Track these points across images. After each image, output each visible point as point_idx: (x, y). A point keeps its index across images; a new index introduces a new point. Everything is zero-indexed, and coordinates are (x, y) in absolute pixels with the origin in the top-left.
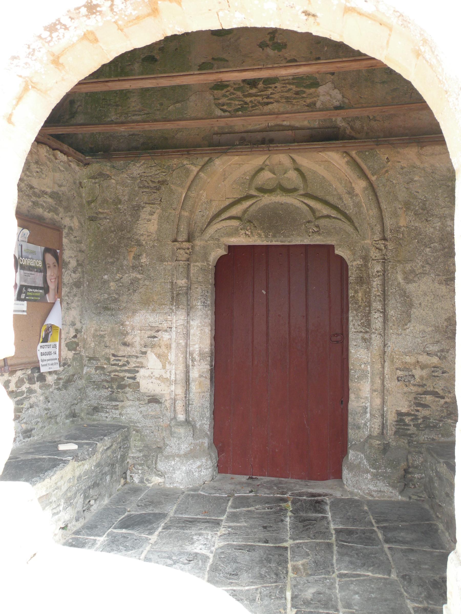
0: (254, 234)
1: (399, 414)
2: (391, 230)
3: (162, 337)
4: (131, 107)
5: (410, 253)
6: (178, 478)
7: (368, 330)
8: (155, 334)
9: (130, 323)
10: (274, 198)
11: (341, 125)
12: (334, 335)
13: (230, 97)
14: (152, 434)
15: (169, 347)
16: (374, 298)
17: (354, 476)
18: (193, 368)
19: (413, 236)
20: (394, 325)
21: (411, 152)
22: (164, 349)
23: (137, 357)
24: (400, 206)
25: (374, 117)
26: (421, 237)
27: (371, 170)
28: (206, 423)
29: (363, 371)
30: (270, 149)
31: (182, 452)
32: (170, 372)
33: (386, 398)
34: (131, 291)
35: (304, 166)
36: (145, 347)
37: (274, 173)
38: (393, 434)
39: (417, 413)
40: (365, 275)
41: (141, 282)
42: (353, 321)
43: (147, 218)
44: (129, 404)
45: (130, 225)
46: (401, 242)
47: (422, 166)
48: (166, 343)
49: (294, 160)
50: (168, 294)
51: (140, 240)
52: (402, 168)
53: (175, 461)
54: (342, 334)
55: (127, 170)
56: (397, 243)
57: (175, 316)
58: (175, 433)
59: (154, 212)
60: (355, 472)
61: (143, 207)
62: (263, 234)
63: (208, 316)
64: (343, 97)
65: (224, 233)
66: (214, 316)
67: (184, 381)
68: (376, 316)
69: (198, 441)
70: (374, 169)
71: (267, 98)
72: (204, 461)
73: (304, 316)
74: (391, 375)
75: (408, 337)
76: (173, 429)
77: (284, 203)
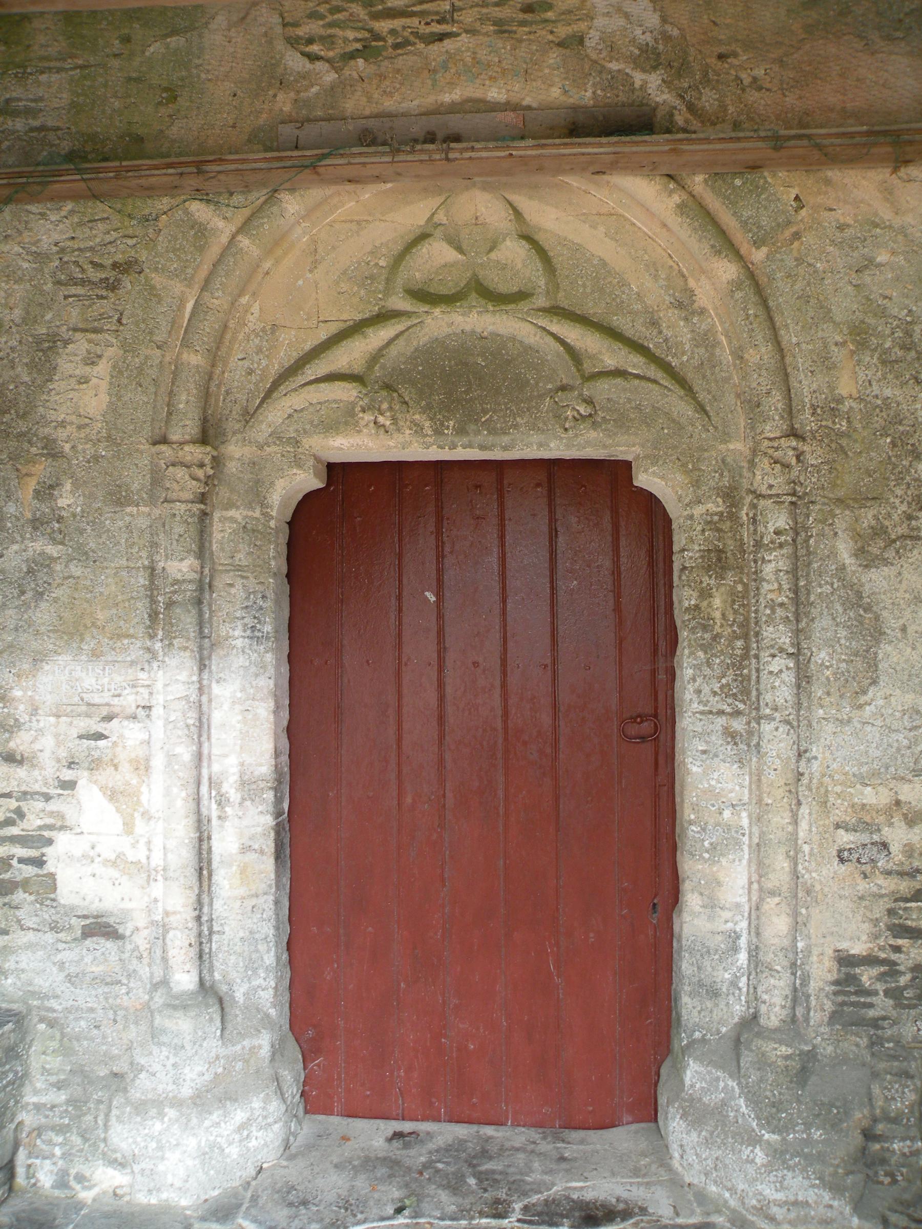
0: (401, 423)
1: (845, 960)
2: (814, 408)
3: (121, 736)
4: (36, 48)
5: (870, 476)
6: (174, 1175)
7: (741, 706)
8: (101, 728)
9: (25, 691)
10: (460, 319)
11: (658, 99)
12: (633, 719)
13: (330, 18)
14: (95, 1031)
15: (142, 766)
16: (768, 611)
17: (707, 1143)
18: (221, 826)
19: (877, 426)
20: (828, 694)
21: (864, 183)
22: (125, 775)
23: (47, 798)
24: (839, 338)
25: (755, 79)
26: (901, 428)
27: (750, 231)
28: (264, 984)
29: (729, 828)
30: (451, 156)
31: (186, 1091)
32: (149, 843)
33: (804, 911)
34: (29, 595)
35: (546, 231)
36: (69, 767)
37: (460, 249)
38: (826, 1019)
39: (894, 957)
40: (731, 545)
41: (58, 568)
42: (694, 680)
43: (77, 372)
44: (25, 940)
45: (27, 396)
46: (844, 442)
47: (897, 222)
48: (133, 755)
49: (517, 213)
50: (139, 605)
51: (55, 441)
52: (841, 228)
53: (163, 1123)
54: (656, 716)
55: (20, 233)
56: (833, 446)
57: (161, 673)
58: (164, 1031)
59: (100, 357)
60: (712, 1133)
61: (66, 342)
62: (427, 424)
63: (264, 667)
64: (664, 20)
65: (311, 422)
66: (285, 669)
67: (191, 872)
68: (774, 667)
69: (239, 1047)
70: (760, 227)
71: (439, 22)
72: (257, 1104)
73: (546, 666)
74: (821, 845)
75: (868, 728)
76: (158, 1020)
77: (491, 334)
